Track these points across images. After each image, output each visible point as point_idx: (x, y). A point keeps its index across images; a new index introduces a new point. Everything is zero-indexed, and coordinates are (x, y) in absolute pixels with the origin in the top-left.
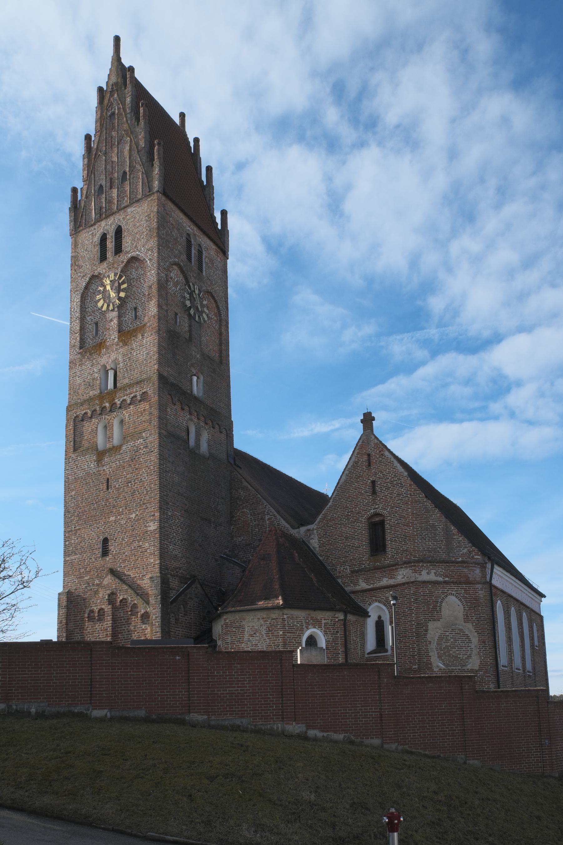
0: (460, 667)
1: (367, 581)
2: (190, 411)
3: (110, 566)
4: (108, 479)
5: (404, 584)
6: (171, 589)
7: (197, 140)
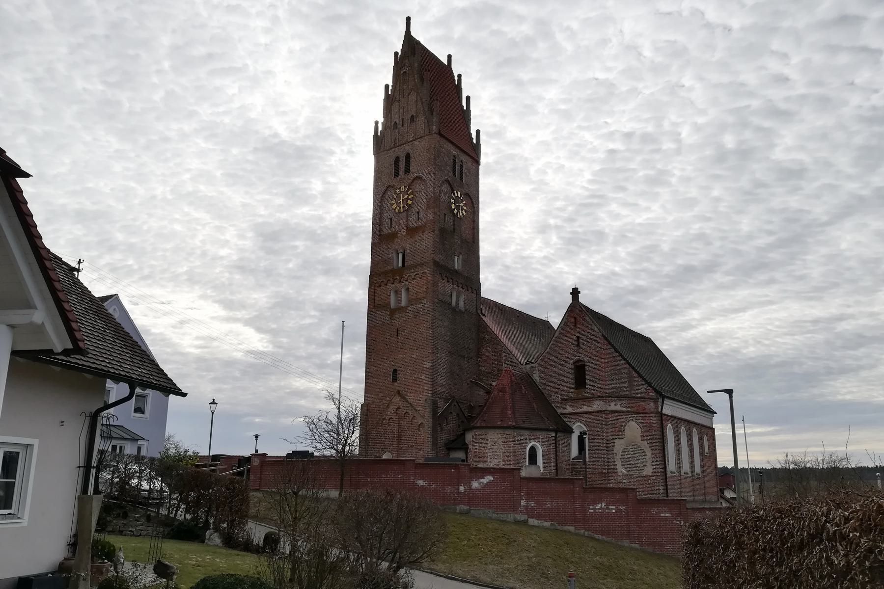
0: (637, 473)
1: (572, 406)
2: (453, 282)
3: (398, 388)
4: (398, 329)
5: (598, 412)
6: (439, 408)
7: (460, 76)
